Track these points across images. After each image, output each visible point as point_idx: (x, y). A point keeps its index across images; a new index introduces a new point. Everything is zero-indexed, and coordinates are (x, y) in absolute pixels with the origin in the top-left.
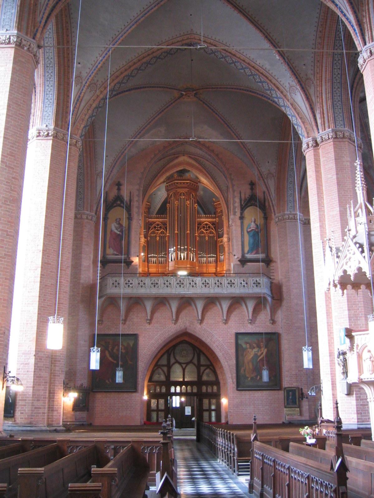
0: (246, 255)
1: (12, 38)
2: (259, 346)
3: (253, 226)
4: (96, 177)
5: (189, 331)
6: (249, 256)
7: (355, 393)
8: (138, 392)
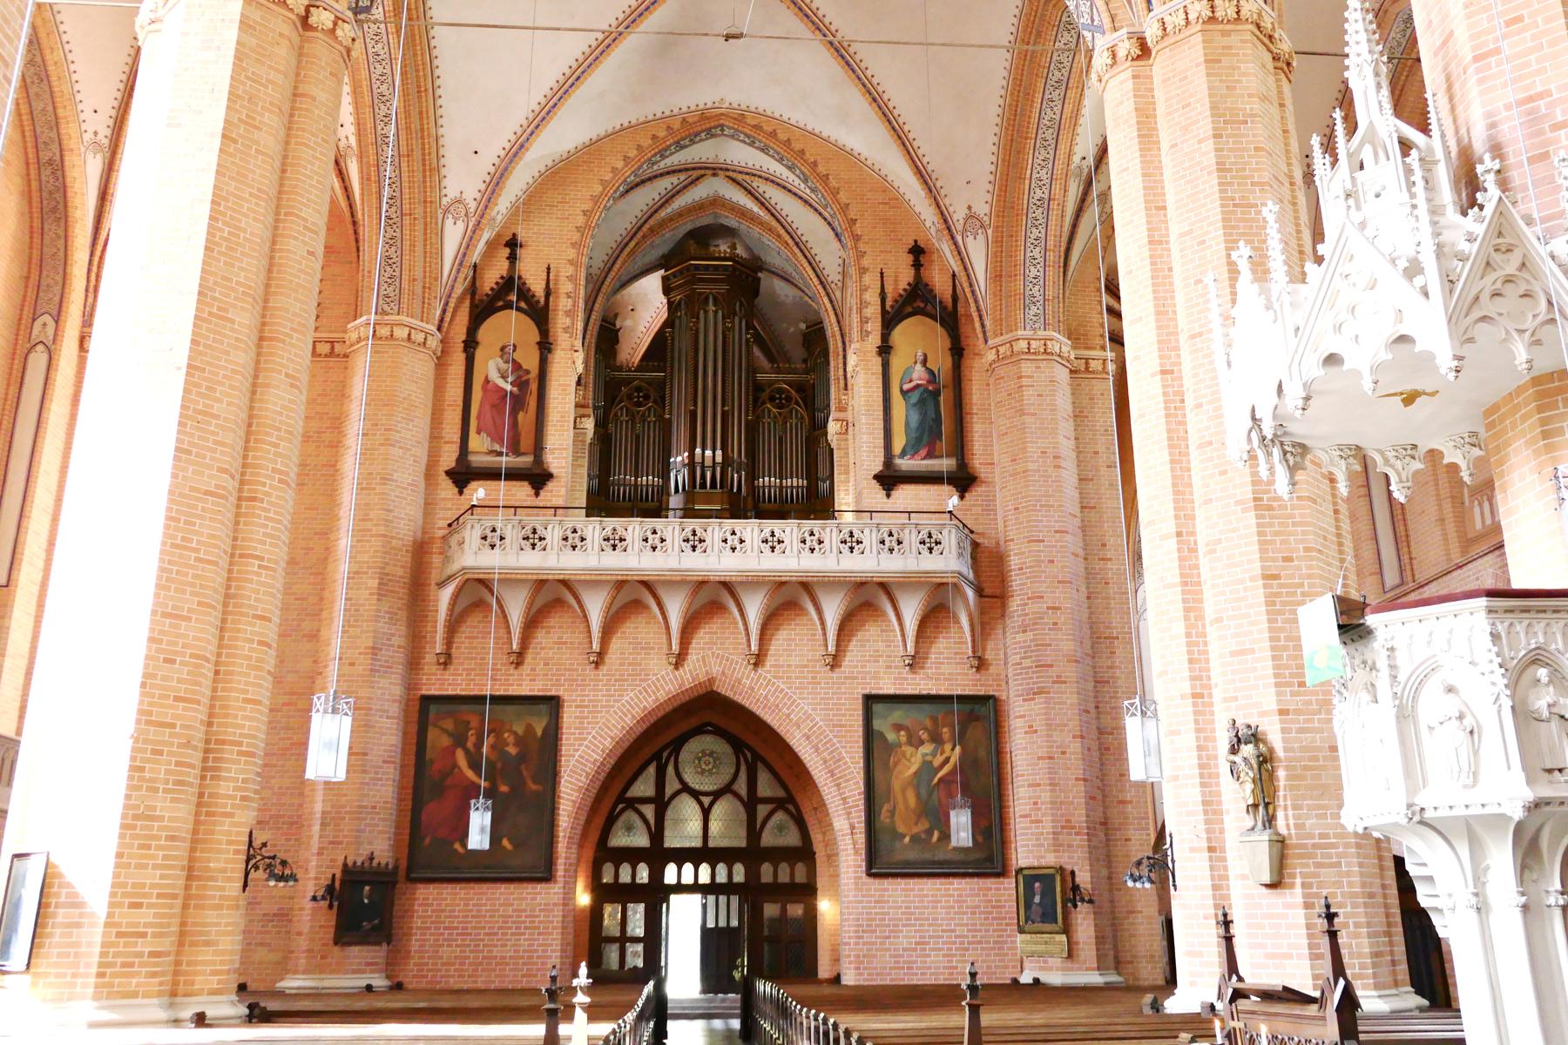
0: (898, 461)
2: (936, 739)
3: (919, 374)
4: (440, 216)
5: (725, 690)
6: (905, 464)
7: (1298, 881)
8: (556, 882)
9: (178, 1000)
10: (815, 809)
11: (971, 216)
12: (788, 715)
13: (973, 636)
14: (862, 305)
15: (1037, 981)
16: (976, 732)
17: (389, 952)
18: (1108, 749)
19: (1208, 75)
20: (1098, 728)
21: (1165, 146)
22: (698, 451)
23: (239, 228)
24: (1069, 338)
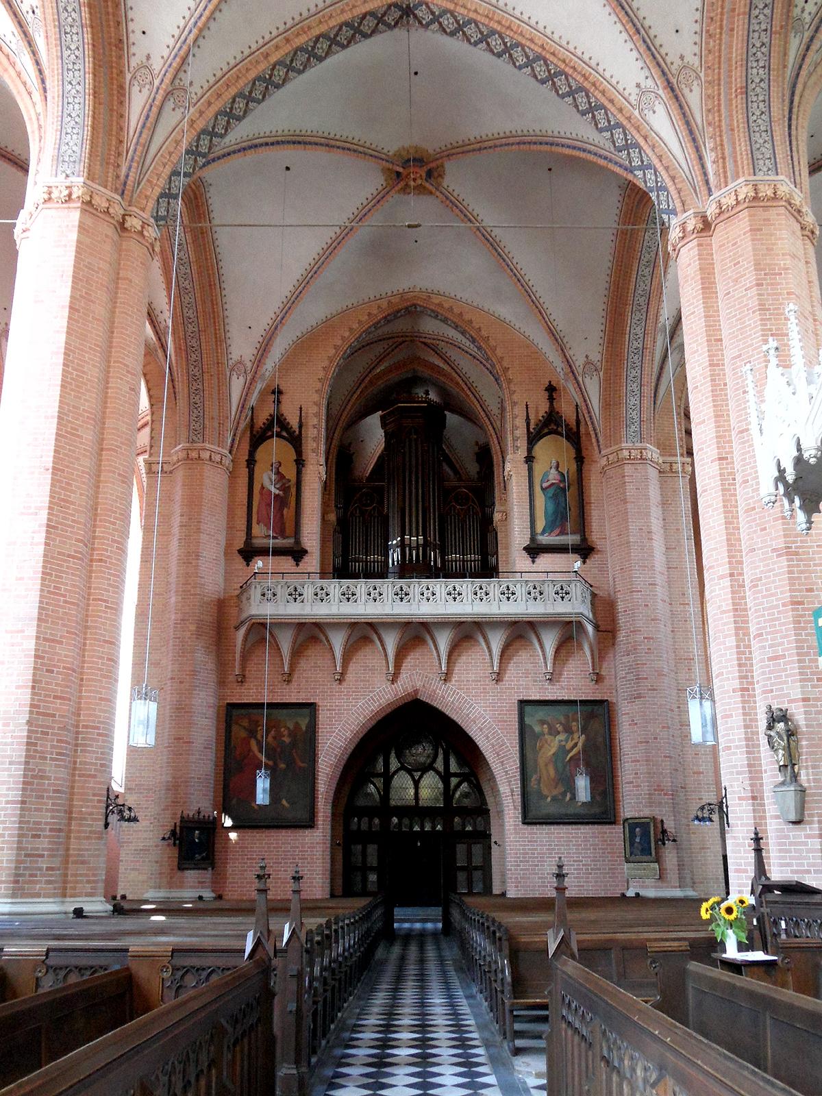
0: (540, 538)
2: (568, 730)
3: (553, 476)
4: (228, 373)
6: (545, 539)
11: (588, 362)
13: (593, 658)
15: (638, 894)
16: (595, 725)
17: (213, 874)
20: (680, 722)
21: (720, 295)
23: (84, 372)
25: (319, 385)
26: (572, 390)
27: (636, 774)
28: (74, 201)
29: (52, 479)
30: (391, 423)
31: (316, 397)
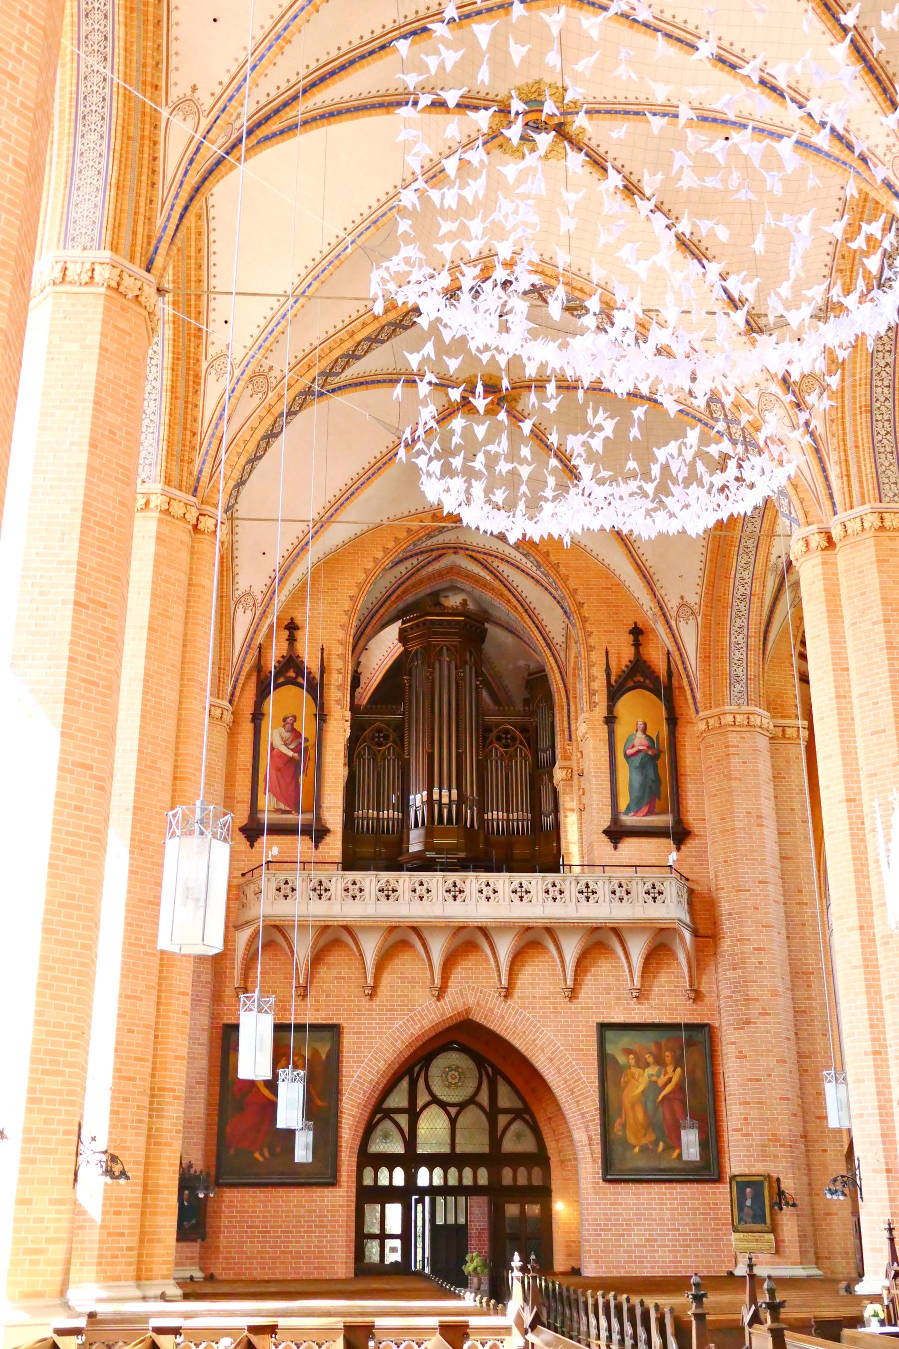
0: (624, 818)
1: (98, 268)
2: (659, 1061)
3: (640, 741)
4: (233, 607)
5: (479, 1018)
6: (630, 820)
8: (340, 1186)
9: (144, 1282)
10: (550, 1119)
11: (683, 605)
12: (534, 1041)
13: (690, 971)
14: (591, 678)
17: (202, 1247)
18: (806, 1071)
19: (879, 572)
20: (798, 1053)
21: (847, 622)
22: (436, 790)
24: (768, 710)
25: (345, 619)
26: (665, 637)
27: (746, 1119)
28: (151, 510)
29: (134, 820)
30: (415, 638)
31: (341, 634)
